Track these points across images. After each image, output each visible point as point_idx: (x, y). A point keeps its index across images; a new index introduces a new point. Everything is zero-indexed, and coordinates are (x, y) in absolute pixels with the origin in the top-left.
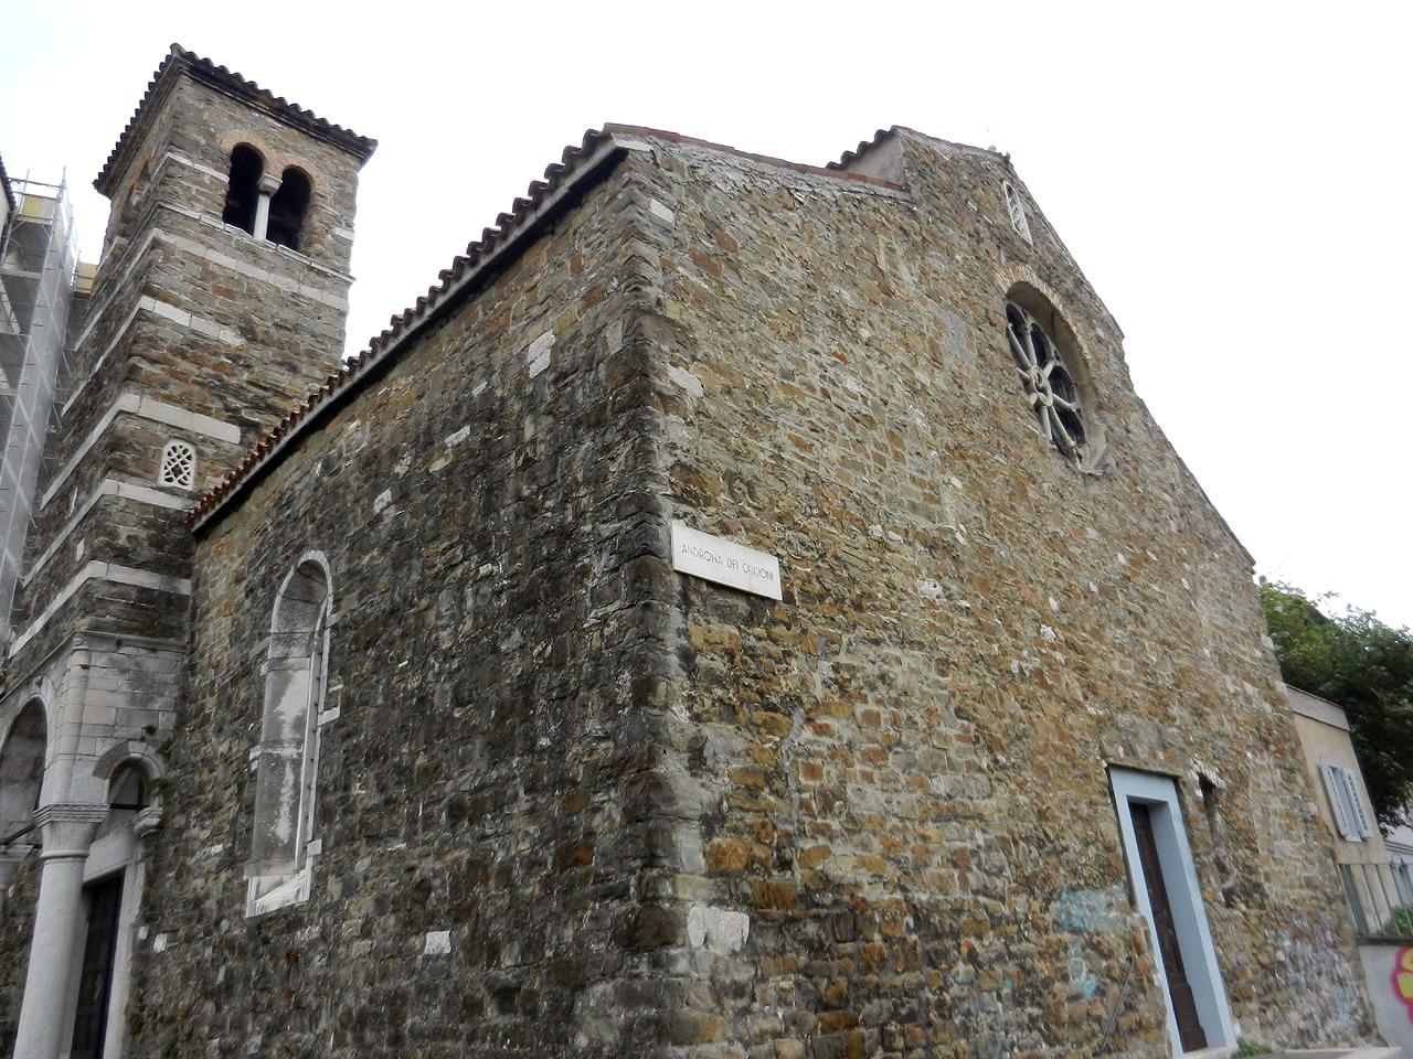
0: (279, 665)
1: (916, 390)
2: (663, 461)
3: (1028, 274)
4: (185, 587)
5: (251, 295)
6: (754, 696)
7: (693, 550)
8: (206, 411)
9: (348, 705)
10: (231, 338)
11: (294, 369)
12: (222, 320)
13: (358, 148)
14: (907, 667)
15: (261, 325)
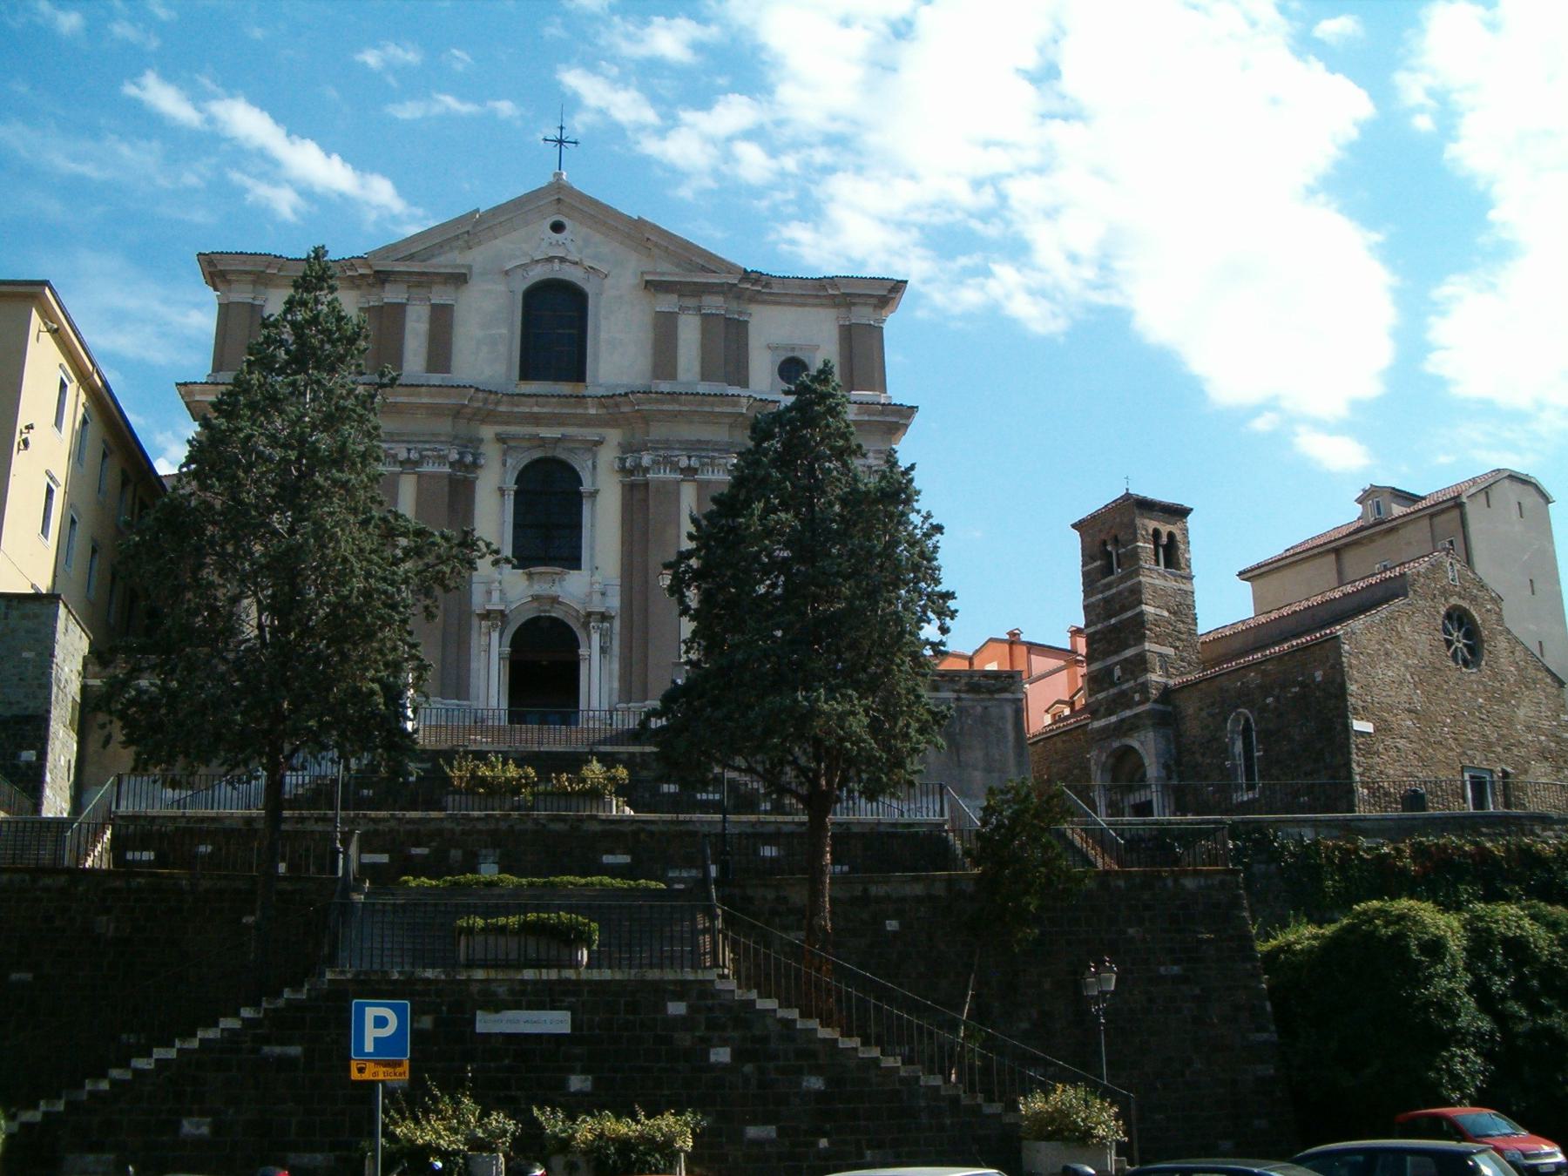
0: (1232, 739)
1: (1407, 667)
3: (1454, 601)
4: (1170, 708)
6: (1369, 752)
7: (1359, 725)
9: (1265, 751)
10: (1166, 614)
13: (1180, 513)
14: (1401, 743)
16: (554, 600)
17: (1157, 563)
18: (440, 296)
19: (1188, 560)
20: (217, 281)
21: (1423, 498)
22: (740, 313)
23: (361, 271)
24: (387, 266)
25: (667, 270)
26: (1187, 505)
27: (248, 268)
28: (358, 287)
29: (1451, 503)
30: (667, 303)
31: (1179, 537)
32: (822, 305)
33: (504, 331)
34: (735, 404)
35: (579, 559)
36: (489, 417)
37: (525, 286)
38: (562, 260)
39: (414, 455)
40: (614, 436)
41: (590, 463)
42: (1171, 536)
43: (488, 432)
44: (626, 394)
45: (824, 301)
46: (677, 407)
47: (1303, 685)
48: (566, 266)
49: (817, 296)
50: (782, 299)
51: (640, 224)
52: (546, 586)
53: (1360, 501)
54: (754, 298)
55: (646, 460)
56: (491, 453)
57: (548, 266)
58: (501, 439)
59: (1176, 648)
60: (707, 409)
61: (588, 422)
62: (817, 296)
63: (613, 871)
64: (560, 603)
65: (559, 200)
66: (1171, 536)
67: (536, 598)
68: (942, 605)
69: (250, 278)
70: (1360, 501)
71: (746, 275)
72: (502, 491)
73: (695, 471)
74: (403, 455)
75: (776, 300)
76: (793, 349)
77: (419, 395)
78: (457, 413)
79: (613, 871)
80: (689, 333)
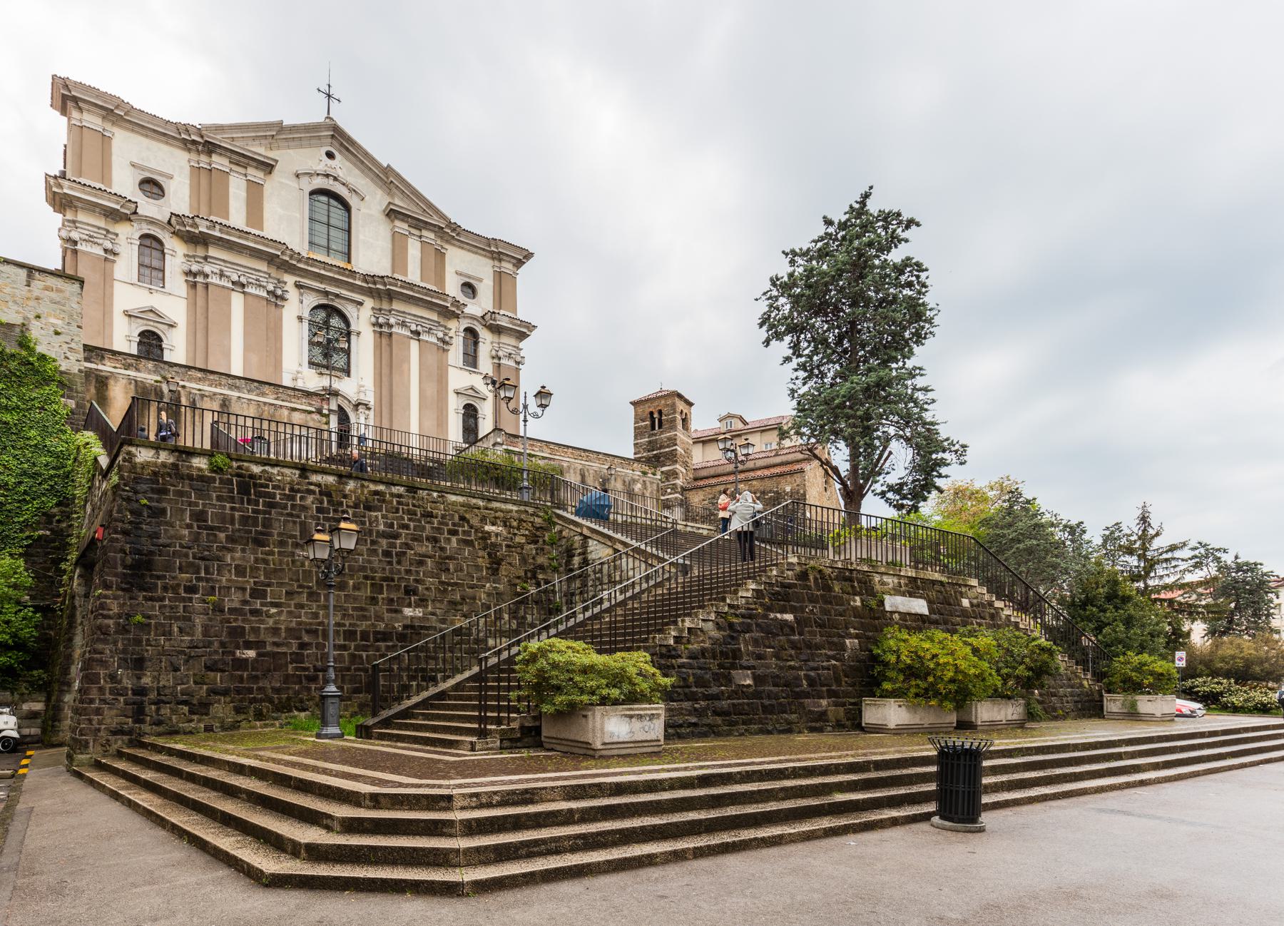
20: (70, 104)
23: (194, 137)
24: (217, 139)
27: (100, 103)
28: (189, 150)
29: (204, 182)
30: (402, 226)
34: (445, 300)
39: (243, 280)
47: (777, 492)
51: (388, 170)
54: (450, 240)
55: (392, 321)
57: (325, 180)
58: (299, 286)
61: (353, 288)
68: (1075, 531)
69: (104, 113)
71: (450, 224)
72: (300, 319)
74: (235, 278)
75: (463, 245)
76: (469, 277)
77: (247, 239)
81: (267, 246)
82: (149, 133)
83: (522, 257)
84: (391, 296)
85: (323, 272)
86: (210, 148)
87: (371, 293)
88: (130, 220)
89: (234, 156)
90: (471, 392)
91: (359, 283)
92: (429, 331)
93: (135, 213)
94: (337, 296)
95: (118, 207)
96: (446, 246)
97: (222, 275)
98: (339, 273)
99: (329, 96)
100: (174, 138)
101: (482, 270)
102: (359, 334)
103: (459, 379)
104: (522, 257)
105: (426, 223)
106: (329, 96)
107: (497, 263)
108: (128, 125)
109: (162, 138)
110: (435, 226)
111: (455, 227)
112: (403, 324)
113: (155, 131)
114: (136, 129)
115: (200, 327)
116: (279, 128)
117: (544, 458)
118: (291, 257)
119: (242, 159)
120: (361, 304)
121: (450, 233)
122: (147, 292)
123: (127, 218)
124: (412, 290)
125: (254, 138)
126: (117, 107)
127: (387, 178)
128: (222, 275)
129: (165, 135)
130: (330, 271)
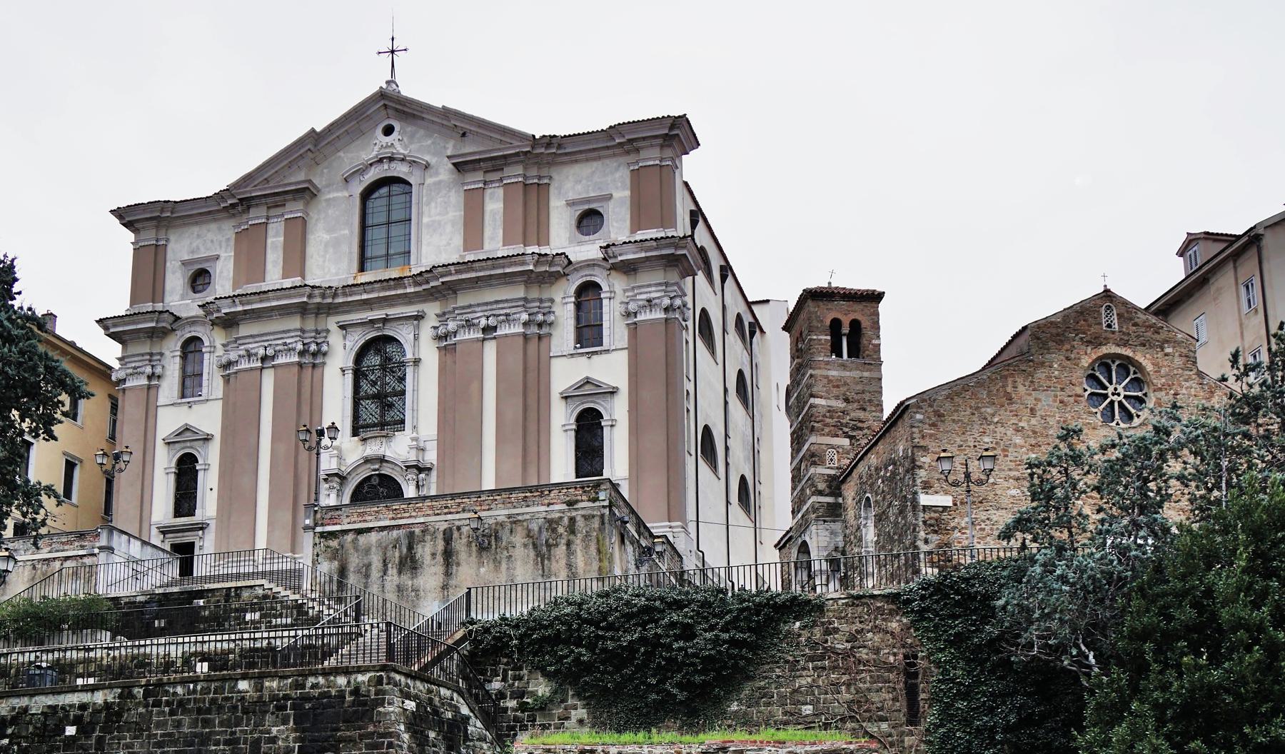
2: (919, 481)
5: (846, 384)
8: (837, 436)
10: (840, 404)
11: (865, 410)
12: (837, 398)
13: (876, 297)
15: (850, 395)
16: (382, 460)
17: (840, 355)
18: (294, 209)
19: (877, 348)
21: (1238, 237)
22: (540, 178)
25: (470, 149)
26: (879, 289)
31: (865, 323)
32: (614, 155)
33: (347, 232)
34: (523, 263)
35: (403, 422)
36: (331, 309)
37: (361, 189)
38: (391, 159)
39: (270, 352)
40: (432, 309)
41: (412, 336)
42: (855, 325)
43: (332, 323)
44: (430, 271)
45: (617, 151)
46: (473, 275)
48: (393, 165)
49: (608, 148)
50: (579, 157)
51: (447, 113)
52: (375, 448)
53: (1181, 253)
56: (335, 338)
59: (851, 438)
60: (500, 271)
61: (408, 299)
62: (608, 148)
63: (85, 689)
64: (387, 462)
65: (385, 105)
66: (855, 325)
67: (367, 460)
69: (154, 223)
70: (1181, 253)
73: (495, 329)
77: (268, 300)
78: (303, 310)
79: (85, 689)
80: (494, 204)
81: (289, 297)
82: (198, 219)
83: (676, 134)
84: (451, 289)
85: (365, 296)
86: (246, 204)
87: (431, 295)
88: (566, 275)
89: (269, 200)
90: (588, 390)
91: (411, 290)
92: (508, 319)
93: (570, 262)
94: (385, 321)
95: (153, 324)
96: (544, 172)
97: (249, 355)
98: (384, 289)
99: (393, 52)
100: (218, 211)
101: (611, 183)
102: (417, 362)
103: (566, 372)
104: (676, 134)
105: (505, 157)
106: (393, 52)
107: (632, 158)
108: (180, 222)
109: (210, 217)
110: (517, 154)
111: (549, 141)
112: (469, 324)
113: (201, 214)
114: (187, 221)
115: (532, 376)
116: (313, 138)
117: (382, 529)
118: (323, 296)
119: (278, 198)
120: (419, 317)
121: (551, 152)
122: (186, 407)
123: (554, 278)
124: (473, 270)
125: (289, 166)
126: (162, 211)
127: (452, 123)
128: (249, 355)
129: (209, 213)
130: (372, 291)
